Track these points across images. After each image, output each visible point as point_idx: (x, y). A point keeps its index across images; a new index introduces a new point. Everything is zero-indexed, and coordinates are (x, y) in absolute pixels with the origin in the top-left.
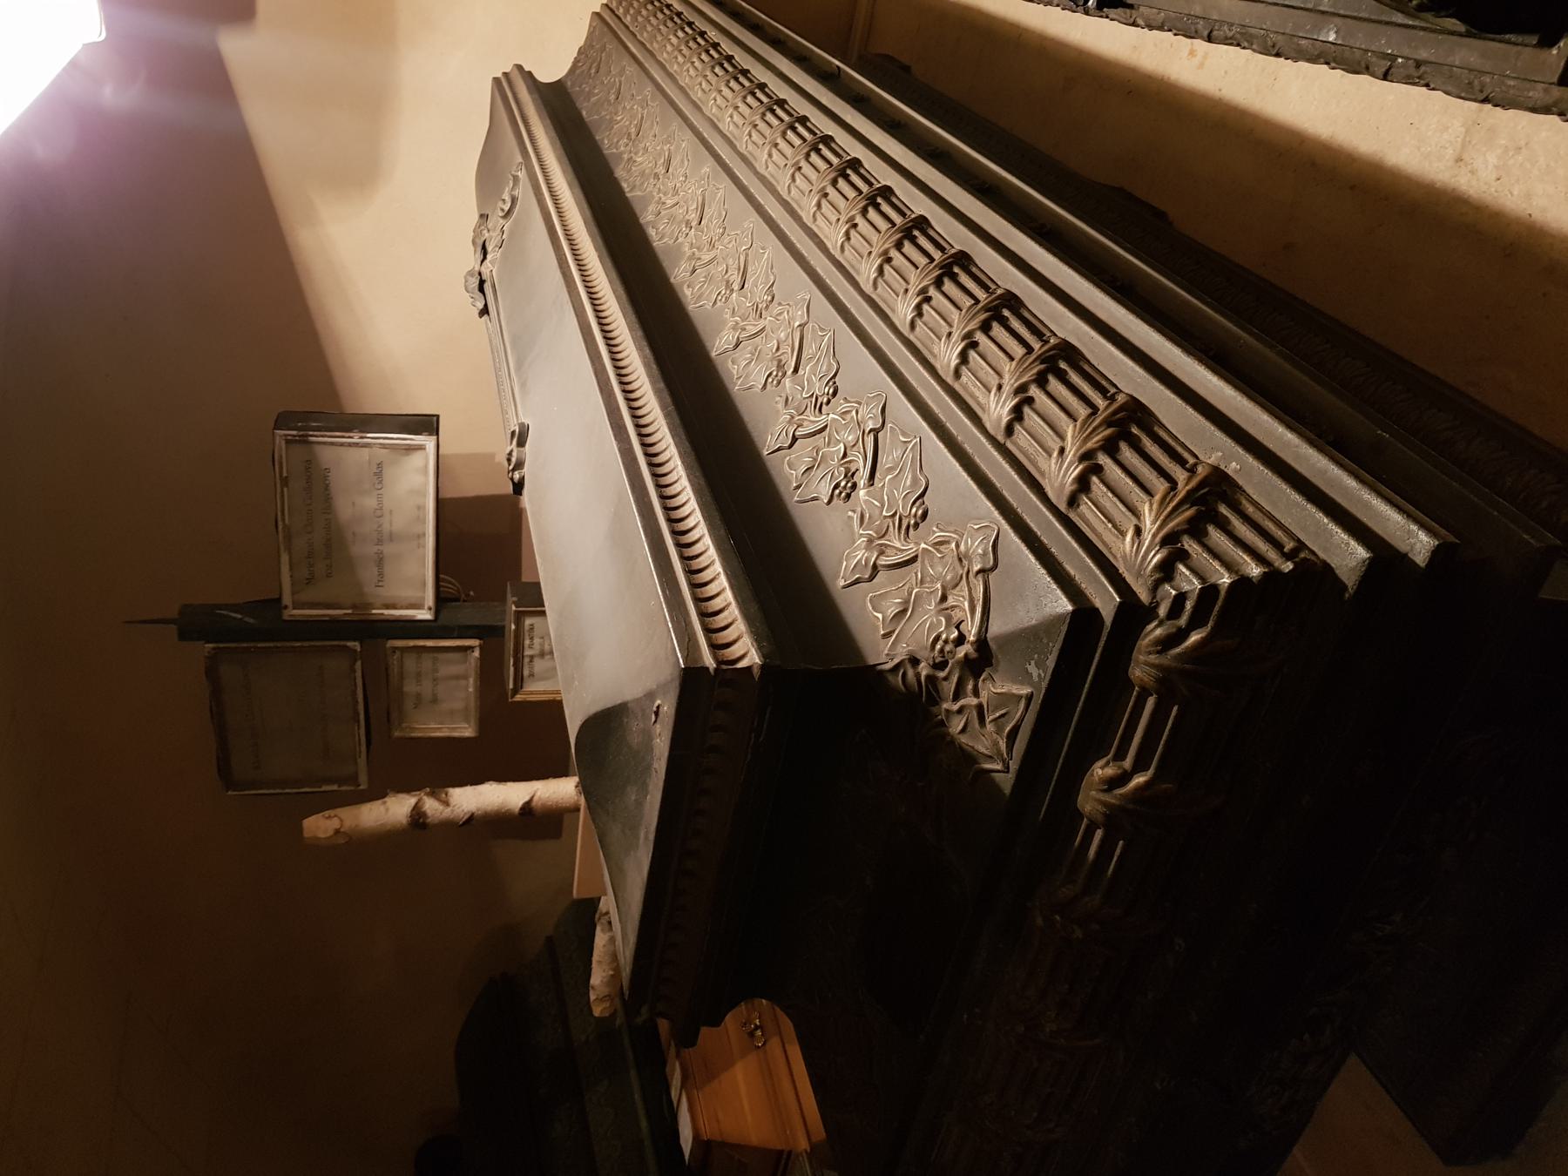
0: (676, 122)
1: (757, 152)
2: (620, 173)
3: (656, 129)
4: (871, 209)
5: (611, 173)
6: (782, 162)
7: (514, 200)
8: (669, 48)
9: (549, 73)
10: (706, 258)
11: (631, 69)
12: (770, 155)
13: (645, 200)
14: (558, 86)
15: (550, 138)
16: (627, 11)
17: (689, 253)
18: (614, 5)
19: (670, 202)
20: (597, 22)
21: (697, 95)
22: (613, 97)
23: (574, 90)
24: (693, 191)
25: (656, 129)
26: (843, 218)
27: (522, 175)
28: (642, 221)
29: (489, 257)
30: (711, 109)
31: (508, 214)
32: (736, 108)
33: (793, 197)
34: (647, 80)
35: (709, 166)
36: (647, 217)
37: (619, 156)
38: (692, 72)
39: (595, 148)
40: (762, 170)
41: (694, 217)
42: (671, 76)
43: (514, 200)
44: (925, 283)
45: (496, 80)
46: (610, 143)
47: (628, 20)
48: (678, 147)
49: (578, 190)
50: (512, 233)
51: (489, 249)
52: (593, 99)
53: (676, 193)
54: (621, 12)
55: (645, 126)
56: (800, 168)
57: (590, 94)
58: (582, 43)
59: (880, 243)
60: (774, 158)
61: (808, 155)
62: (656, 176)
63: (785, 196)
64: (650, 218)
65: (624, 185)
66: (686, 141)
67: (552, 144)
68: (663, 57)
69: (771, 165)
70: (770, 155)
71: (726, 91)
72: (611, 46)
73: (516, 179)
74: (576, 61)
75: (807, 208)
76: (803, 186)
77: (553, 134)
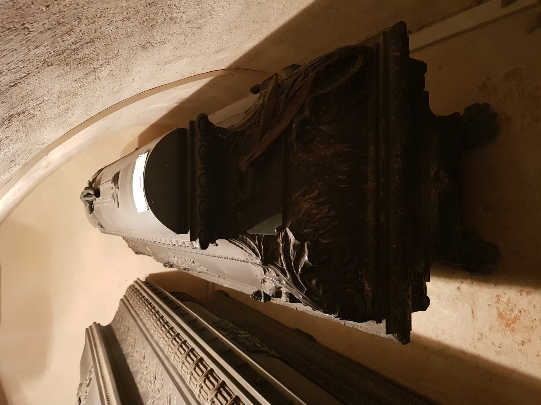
0: (146, 342)
1: (171, 355)
2: (128, 361)
3: (140, 344)
4: (219, 395)
5: (126, 361)
6: (178, 360)
7: (90, 380)
8: (143, 314)
9: (105, 323)
10: (157, 397)
11: (132, 320)
12: (175, 357)
13: (137, 372)
14: (109, 327)
15: (103, 352)
16: (131, 299)
17: (151, 395)
18: (127, 296)
19: (145, 373)
20: (122, 303)
21: (152, 332)
22: (126, 330)
23: (114, 327)
24: (152, 369)
25: (140, 344)
26: (210, 399)
27: (93, 370)
28: (136, 381)
29: (82, 403)
30: (156, 338)
31: (88, 385)
32: (164, 338)
33: (182, 373)
34: (136, 326)
35: (156, 360)
36: (137, 380)
37: (128, 354)
38: (150, 323)
39: (120, 350)
40: (172, 363)
41: (153, 379)
42: (133, 308)
43: (90, 380)
44: (212, 397)
45: (122, 300)
46: (126, 349)
47: (131, 302)
48: (147, 351)
49: (112, 375)
50: (89, 393)
51: (82, 399)
52: (121, 331)
53: (147, 369)
54: (129, 299)
55: (137, 342)
56: (184, 363)
57: (119, 329)
58: (117, 310)
59: (211, 395)
60: (176, 358)
61: (186, 358)
62: (141, 362)
63: (180, 373)
64: (139, 380)
65: (130, 366)
66: (149, 350)
67: (104, 355)
68: (141, 317)
69: (183, 372)
70: (175, 357)
71: (161, 331)
72: (126, 311)
73: (91, 372)
74: (115, 316)
75: (187, 378)
76: (185, 368)
77: (105, 350)
